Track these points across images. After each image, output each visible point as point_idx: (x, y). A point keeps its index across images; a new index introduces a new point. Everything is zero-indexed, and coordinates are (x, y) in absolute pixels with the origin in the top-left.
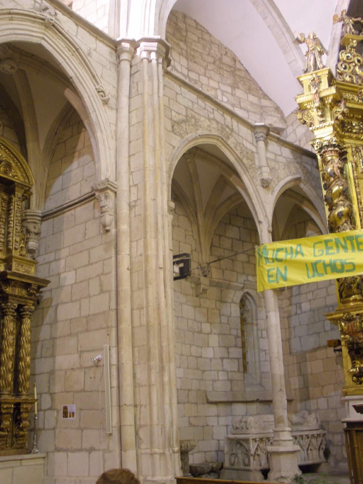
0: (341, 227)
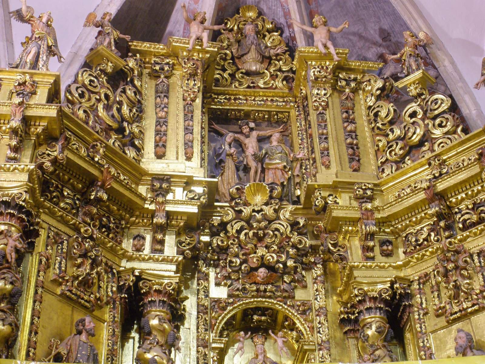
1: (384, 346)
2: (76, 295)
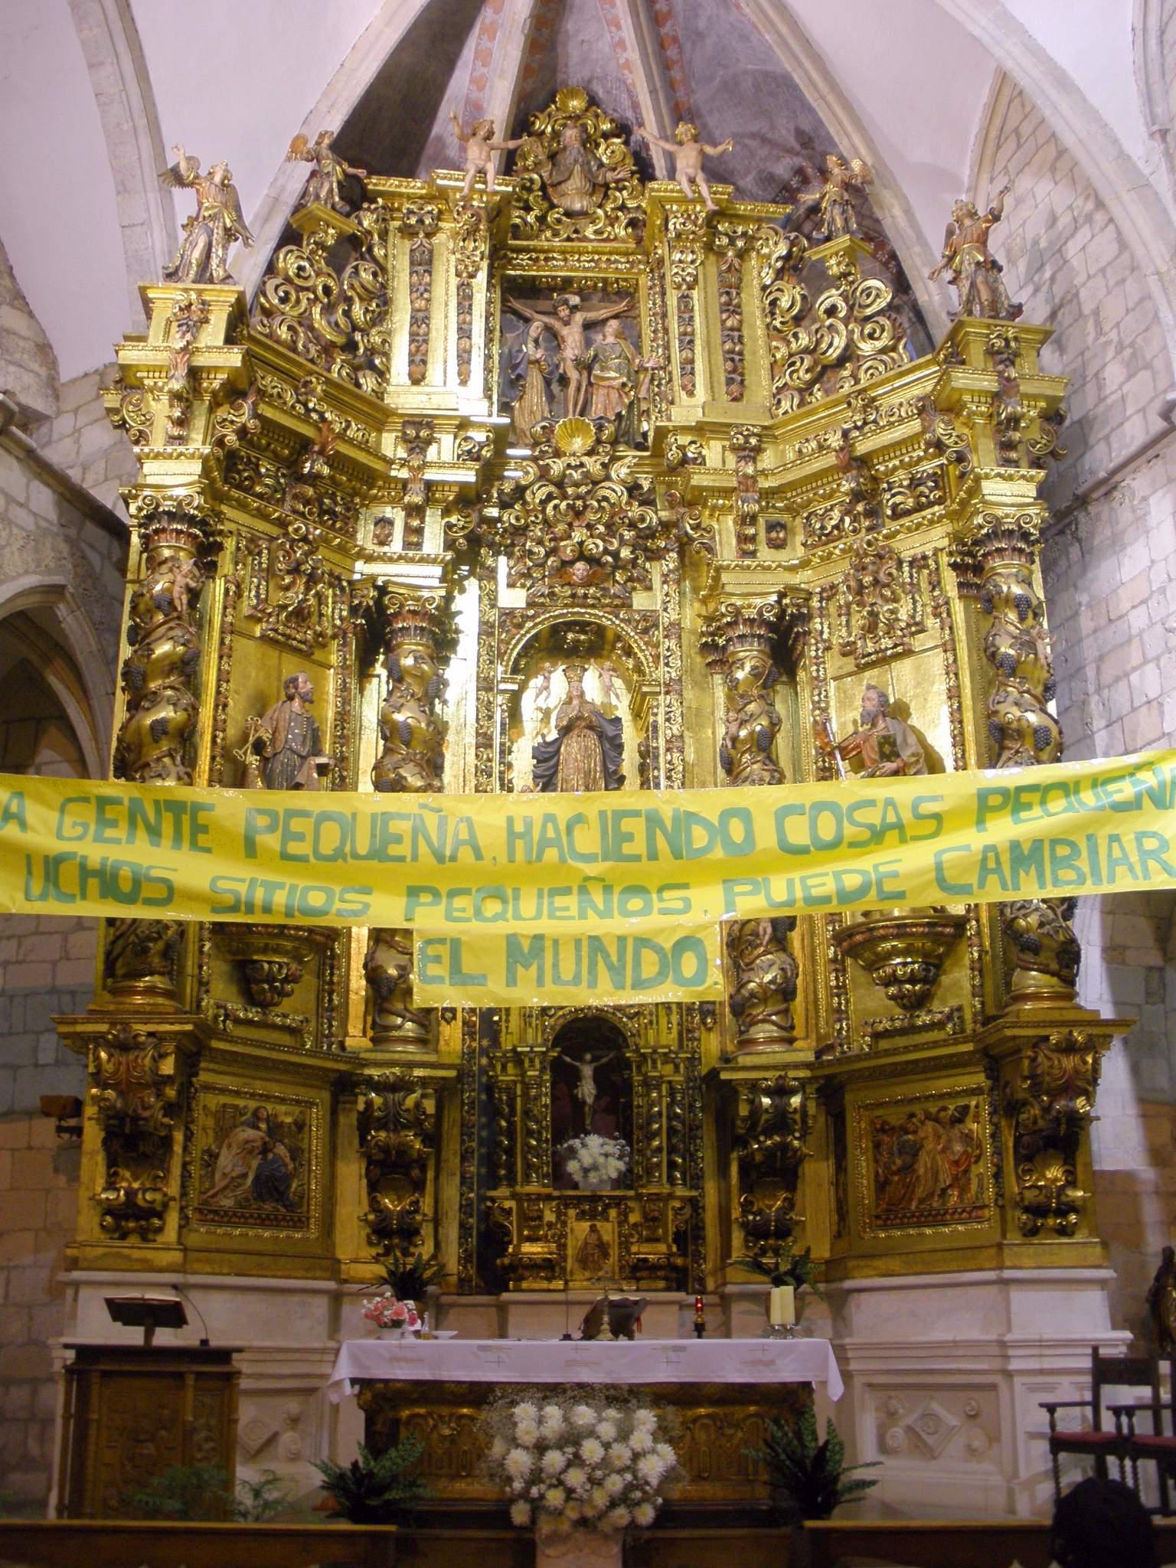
0: (153, 765)
1: (761, 697)
2: (283, 635)
